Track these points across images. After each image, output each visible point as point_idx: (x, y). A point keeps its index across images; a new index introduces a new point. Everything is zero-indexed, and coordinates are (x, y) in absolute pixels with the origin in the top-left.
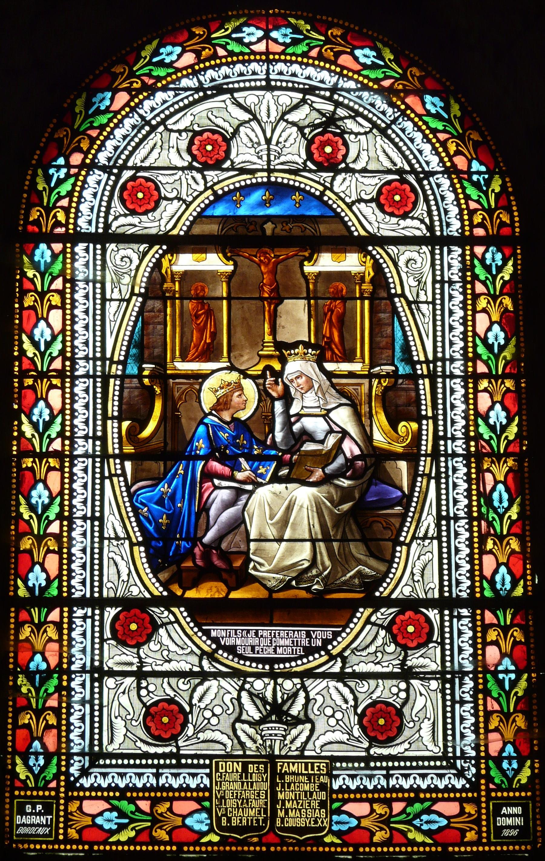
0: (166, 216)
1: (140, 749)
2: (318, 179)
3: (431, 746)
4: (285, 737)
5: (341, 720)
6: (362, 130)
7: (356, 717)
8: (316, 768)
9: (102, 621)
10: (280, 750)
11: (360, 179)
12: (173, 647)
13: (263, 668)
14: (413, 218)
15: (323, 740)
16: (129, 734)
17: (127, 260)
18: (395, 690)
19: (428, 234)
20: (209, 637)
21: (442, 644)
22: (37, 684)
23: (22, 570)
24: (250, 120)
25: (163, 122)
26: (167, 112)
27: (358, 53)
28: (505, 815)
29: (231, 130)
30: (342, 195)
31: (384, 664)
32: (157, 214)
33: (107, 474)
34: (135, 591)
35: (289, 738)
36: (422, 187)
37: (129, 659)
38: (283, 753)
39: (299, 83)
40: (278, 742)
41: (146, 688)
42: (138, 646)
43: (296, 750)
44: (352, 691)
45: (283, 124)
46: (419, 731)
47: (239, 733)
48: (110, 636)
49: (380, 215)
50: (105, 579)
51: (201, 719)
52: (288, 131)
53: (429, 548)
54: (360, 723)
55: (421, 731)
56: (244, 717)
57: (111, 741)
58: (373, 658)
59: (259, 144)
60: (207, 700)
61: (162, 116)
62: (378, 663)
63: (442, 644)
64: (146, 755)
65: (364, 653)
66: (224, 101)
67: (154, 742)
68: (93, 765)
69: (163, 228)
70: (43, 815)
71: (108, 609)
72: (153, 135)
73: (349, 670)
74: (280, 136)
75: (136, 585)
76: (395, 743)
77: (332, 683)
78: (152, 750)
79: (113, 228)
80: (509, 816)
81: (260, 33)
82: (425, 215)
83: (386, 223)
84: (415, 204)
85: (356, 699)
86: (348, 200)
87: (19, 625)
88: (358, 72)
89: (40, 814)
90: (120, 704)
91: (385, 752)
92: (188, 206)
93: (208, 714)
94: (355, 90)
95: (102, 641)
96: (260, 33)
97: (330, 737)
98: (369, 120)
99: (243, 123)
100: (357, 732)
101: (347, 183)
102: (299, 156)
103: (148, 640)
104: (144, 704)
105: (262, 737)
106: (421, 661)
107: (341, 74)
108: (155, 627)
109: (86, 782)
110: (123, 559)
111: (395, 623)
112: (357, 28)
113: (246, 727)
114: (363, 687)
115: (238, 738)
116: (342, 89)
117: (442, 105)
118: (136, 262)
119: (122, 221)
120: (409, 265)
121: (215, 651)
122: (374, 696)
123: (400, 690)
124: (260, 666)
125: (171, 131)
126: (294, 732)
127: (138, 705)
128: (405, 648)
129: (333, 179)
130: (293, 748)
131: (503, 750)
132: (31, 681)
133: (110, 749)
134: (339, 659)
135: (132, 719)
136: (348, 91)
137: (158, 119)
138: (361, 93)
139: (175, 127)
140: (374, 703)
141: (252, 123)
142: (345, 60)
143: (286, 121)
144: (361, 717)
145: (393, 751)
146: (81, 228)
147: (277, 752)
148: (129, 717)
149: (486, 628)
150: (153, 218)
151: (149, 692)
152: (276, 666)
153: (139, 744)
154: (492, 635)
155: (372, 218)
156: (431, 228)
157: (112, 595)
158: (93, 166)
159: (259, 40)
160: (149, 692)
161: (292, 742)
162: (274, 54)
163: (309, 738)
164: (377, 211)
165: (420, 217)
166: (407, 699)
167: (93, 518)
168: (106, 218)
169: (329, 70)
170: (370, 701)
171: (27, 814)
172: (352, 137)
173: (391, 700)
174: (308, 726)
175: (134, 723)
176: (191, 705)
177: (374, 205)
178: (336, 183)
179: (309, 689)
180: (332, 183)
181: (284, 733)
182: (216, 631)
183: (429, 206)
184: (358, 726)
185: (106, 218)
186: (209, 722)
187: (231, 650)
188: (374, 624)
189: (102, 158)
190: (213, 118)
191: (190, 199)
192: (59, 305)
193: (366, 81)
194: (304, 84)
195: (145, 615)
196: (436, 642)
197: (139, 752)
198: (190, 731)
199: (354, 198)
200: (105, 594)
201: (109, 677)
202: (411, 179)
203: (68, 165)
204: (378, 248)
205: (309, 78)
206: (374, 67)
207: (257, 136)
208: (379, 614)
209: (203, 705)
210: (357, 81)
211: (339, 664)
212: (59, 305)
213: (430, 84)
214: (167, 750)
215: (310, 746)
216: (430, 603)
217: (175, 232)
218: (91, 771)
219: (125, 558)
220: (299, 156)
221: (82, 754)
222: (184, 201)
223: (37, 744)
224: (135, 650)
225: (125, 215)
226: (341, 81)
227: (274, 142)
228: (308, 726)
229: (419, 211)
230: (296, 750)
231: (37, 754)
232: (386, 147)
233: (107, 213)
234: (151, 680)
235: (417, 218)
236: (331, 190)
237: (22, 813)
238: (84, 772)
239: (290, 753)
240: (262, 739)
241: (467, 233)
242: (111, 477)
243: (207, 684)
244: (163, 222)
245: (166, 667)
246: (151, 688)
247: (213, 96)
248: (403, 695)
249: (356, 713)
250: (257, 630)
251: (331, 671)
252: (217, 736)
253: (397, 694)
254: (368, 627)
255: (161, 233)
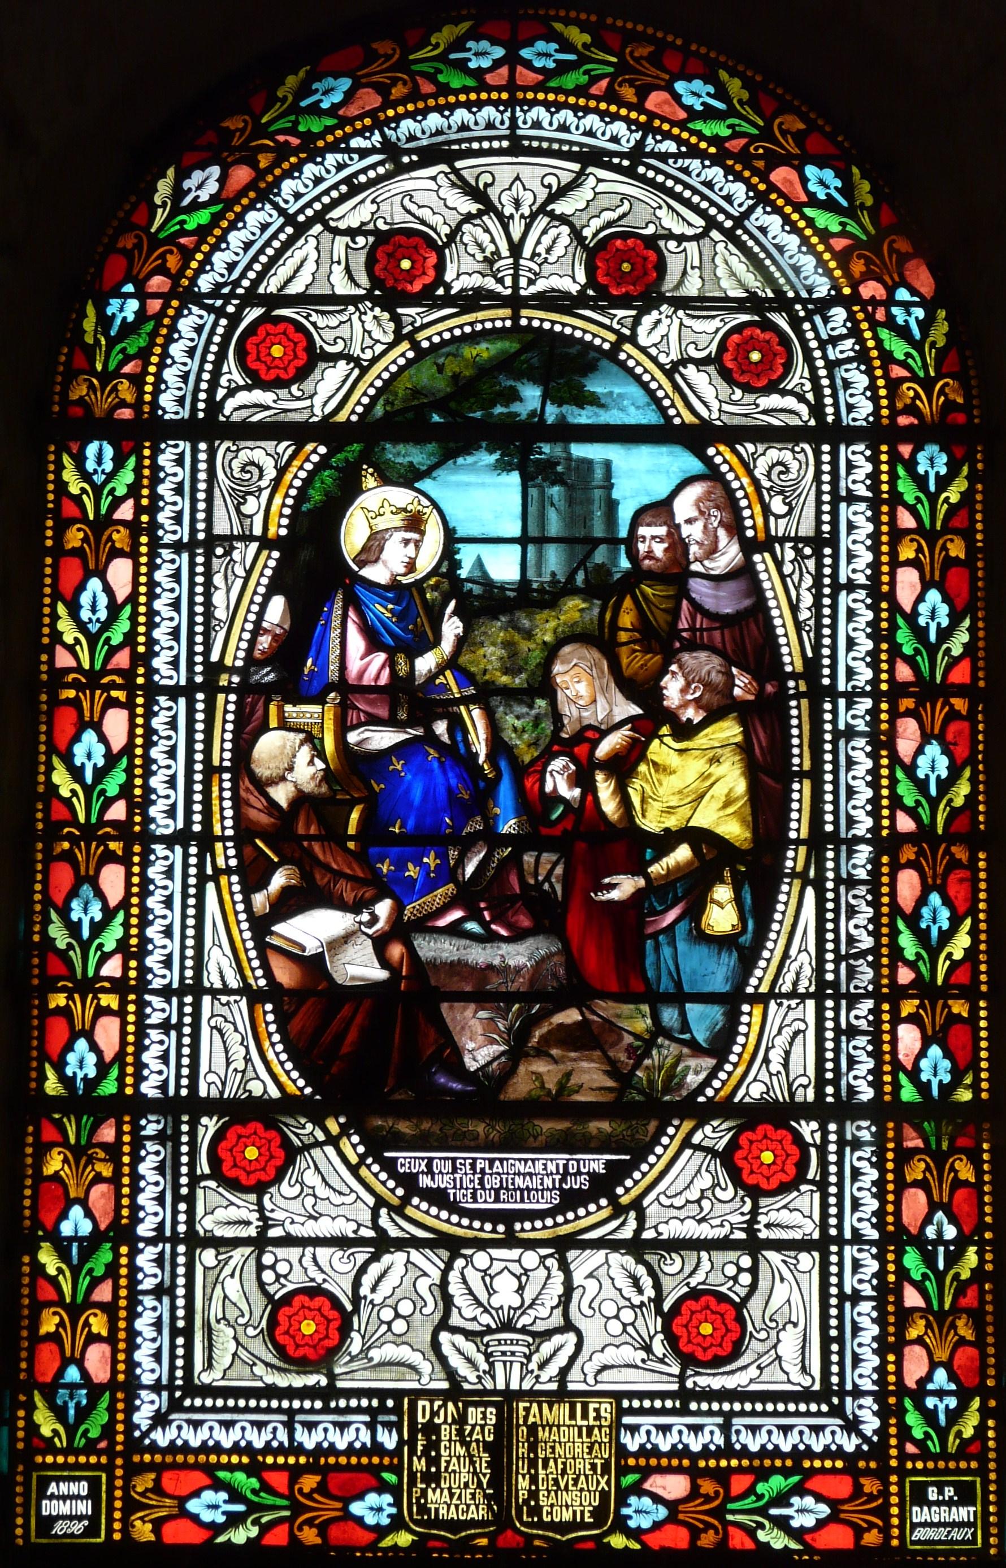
0: (325, 389)
1: (261, 1379)
2: (607, 322)
3: (796, 1376)
4: (529, 1358)
5: (632, 1324)
6: (690, 232)
7: (659, 1320)
8: (592, 1414)
9: (193, 1144)
10: (522, 1379)
11: (687, 321)
12: (322, 1191)
13: (494, 1231)
14: (784, 393)
15: (599, 1359)
16: (242, 1352)
17: (256, 472)
18: (731, 1270)
19: (812, 423)
20: (393, 1174)
21: (822, 1186)
22: (75, 1261)
23: (54, 1047)
24: (480, 214)
25: (320, 217)
26: (326, 200)
27: (680, 86)
28: (52, 1497)
29: (445, 230)
30: (653, 351)
31: (714, 1222)
32: (308, 385)
33: (209, 871)
34: (256, 1088)
35: (535, 1358)
36: (800, 334)
37: (244, 1214)
38: (526, 1386)
39: (571, 143)
40: (516, 1367)
41: (273, 1267)
42: (260, 1189)
43: (550, 1381)
44: (652, 1272)
45: (542, 222)
46: (775, 1347)
47: (447, 1350)
48: (207, 1171)
49: (724, 389)
50: (204, 1068)
51: (374, 1321)
52: (553, 232)
53: (798, 1014)
54: (667, 1331)
55: (780, 1347)
56: (455, 1320)
57: (209, 1365)
58: (694, 1209)
59: (497, 252)
60: (385, 1288)
61: (317, 206)
62: (703, 1220)
63: (822, 1186)
64: (271, 1392)
65: (678, 1202)
66: (434, 178)
67: (281, 1364)
68: (176, 1405)
69: (317, 411)
70: (958, 1504)
71: (204, 1120)
72: (302, 241)
73: (648, 1235)
74: (538, 242)
75: (258, 1078)
76: (728, 1368)
77: (615, 1258)
78: (282, 1381)
79: (227, 411)
80: (64, 1498)
81: (499, 52)
82: (808, 386)
83: (735, 403)
84: (788, 367)
85: (657, 1286)
86: (663, 359)
87: (42, 1151)
88: (682, 125)
89: (950, 1503)
90: (225, 1297)
91: (716, 1383)
92: (364, 371)
93: (387, 1314)
94: (676, 156)
95: (195, 1180)
96: (499, 52)
97: (610, 1356)
98: (702, 213)
99: (468, 218)
100: (659, 1347)
101: (662, 329)
102: (573, 278)
103: (278, 1179)
104: (269, 1297)
105: (488, 1356)
106: (784, 1217)
107: (647, 129)
108: (291, 1153)
109: (162, 1438)
110: (236, 1030)
111: (739, 1147)
112: (679, 42)
113: (459, 1339)
114: (673, 1265)
115: (443, 1360)
116: (653, 155)
117: (839, 184)
118: (271, 473)
119: (243, 397)
120: (774, 477)
121: (406, 1200)
122: (693, 1282)
123: (740, 1270)
124: (488, 1227)
125: (336, 232)
126: (547, 1348)
127: (259, 1302)
128: (755, 1193)
129: (637, 321)
130: (545, 1376)
131: (929, 1377)
132: (63, 1254)
133: (206, 1378)
134: (632, 1214)
135: (246, 1325)
136: (663, 157)
137: (309, 212)
138: (687, 162)
139: (342, 225)
140: (694, 1294)
141: (485, 218)
142: (655, 100)
143: (551, 214)
144: (668, 1319)
145: (730, 1382)
146: (165, 412)
147: (514, 1386)
148: (241, 1321)
149: (904, 1156)
150: (299, 394)
151: (278, 1276)
152: (518, 1226)
153: (259, 1370)
154: (916, 1171)
155: (709, 393)
156: (817, 410)
157: (214, 1093)
158: (191, 297)
159: (497, 64)
160: (278, 1276)
161: (542, 1366)
162: (525, 89)
163: (572, 1359)
164: (719, 381)
165: (798, 389)
166: (753, 1287)
167: (837, 588)
168: (212, 391)
169: (626, 120)
170: (686, 1289)
171: (930, 1504)
172: (672, 245)
173: (723, 1289)
174: (571, 1338)
175: (251, 1331)
176: (356, 1299)
177: (711, 369)
178: (642, 331)
179: (572, 1267)
180: (634, 329)
181: (526, 1351)
182: (408, 1160)
183: (813, 370)
184: (661, 1336)
185: (212, 391)
186: (389, 1329)
187: (438, 1198)
188: (698, 1148)
189: (205, 283)
190: (413, 208)
191: (368, 355)
192: (127, 549)
193: (694, 140)
194: (581, 145)
195: (273, 1134)
196: (812, 1182)
197: (260, 1384)
198: (356, 1345)
199: (675, 356)
200: (203, 1093)
201: (204, 1248)
202: (781, 321)
203: (142, 295)
204: (722, 448)
205: (590, 133)
206: (709, 114)
207: (493, 241)
208: (708, 1129)
209: (378, 1298)
210: (678, 140)
211: (632, 1224)
212: (127, 549)
213: (815, 143)
214: (311, 1380)
215: (575, 1374)
216: (805, 1111)
217: (342, 417)
218: (172, 1417)
219: (241, 1029)
220: (573, 278)
221: (156, 1387)
222: (357, 361)
223: (73, 1374)
224: (253, 1197)
225: (248, 388)
226: (650, 140)
227: (527, 252)
228: (571, 1338)
229: (796, 380)
230: (550, 1381)
231: (72, 1387)
232: (734, 261)
233: (214, 383)
234: (282, 1252)
235: (791, 393)
236: (633, 340)
237: (920, 1498)
238: (160, 1420)
239: (537, 1387)
240: (487, 1360)
241: (885, 421)
242: (215, 878)
243: (387, 1259)
244: (318, 401)
245: (311, 1229)
246: (282, 1268)
247: (412, 167)
248: (746, 1279)
249: (659, 1311)
250: (475, 1160)
251: (620, 1236)
252: (403, 1353)
253: (735, 1279)
254: (688, 1152)
255: (315, 419)
